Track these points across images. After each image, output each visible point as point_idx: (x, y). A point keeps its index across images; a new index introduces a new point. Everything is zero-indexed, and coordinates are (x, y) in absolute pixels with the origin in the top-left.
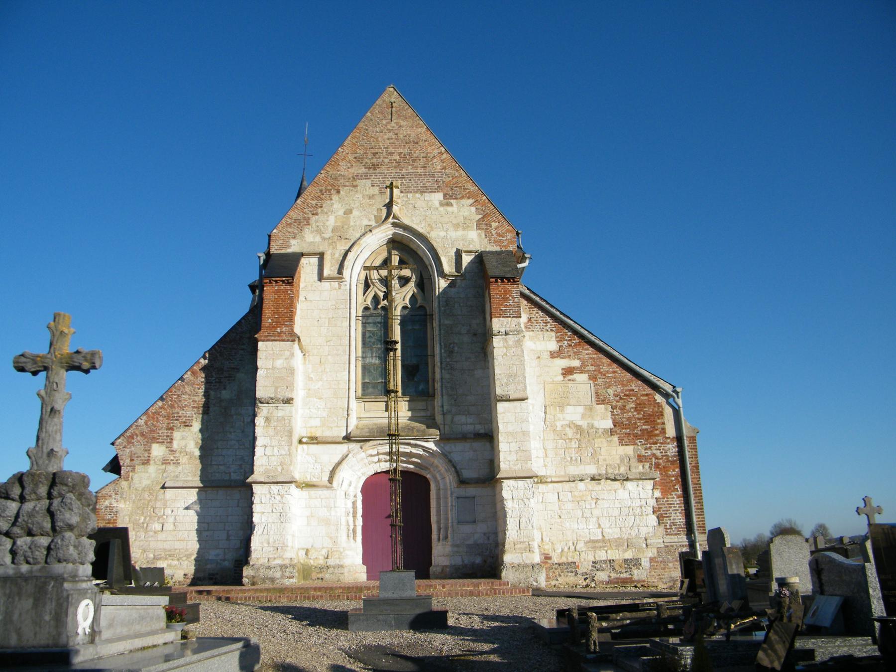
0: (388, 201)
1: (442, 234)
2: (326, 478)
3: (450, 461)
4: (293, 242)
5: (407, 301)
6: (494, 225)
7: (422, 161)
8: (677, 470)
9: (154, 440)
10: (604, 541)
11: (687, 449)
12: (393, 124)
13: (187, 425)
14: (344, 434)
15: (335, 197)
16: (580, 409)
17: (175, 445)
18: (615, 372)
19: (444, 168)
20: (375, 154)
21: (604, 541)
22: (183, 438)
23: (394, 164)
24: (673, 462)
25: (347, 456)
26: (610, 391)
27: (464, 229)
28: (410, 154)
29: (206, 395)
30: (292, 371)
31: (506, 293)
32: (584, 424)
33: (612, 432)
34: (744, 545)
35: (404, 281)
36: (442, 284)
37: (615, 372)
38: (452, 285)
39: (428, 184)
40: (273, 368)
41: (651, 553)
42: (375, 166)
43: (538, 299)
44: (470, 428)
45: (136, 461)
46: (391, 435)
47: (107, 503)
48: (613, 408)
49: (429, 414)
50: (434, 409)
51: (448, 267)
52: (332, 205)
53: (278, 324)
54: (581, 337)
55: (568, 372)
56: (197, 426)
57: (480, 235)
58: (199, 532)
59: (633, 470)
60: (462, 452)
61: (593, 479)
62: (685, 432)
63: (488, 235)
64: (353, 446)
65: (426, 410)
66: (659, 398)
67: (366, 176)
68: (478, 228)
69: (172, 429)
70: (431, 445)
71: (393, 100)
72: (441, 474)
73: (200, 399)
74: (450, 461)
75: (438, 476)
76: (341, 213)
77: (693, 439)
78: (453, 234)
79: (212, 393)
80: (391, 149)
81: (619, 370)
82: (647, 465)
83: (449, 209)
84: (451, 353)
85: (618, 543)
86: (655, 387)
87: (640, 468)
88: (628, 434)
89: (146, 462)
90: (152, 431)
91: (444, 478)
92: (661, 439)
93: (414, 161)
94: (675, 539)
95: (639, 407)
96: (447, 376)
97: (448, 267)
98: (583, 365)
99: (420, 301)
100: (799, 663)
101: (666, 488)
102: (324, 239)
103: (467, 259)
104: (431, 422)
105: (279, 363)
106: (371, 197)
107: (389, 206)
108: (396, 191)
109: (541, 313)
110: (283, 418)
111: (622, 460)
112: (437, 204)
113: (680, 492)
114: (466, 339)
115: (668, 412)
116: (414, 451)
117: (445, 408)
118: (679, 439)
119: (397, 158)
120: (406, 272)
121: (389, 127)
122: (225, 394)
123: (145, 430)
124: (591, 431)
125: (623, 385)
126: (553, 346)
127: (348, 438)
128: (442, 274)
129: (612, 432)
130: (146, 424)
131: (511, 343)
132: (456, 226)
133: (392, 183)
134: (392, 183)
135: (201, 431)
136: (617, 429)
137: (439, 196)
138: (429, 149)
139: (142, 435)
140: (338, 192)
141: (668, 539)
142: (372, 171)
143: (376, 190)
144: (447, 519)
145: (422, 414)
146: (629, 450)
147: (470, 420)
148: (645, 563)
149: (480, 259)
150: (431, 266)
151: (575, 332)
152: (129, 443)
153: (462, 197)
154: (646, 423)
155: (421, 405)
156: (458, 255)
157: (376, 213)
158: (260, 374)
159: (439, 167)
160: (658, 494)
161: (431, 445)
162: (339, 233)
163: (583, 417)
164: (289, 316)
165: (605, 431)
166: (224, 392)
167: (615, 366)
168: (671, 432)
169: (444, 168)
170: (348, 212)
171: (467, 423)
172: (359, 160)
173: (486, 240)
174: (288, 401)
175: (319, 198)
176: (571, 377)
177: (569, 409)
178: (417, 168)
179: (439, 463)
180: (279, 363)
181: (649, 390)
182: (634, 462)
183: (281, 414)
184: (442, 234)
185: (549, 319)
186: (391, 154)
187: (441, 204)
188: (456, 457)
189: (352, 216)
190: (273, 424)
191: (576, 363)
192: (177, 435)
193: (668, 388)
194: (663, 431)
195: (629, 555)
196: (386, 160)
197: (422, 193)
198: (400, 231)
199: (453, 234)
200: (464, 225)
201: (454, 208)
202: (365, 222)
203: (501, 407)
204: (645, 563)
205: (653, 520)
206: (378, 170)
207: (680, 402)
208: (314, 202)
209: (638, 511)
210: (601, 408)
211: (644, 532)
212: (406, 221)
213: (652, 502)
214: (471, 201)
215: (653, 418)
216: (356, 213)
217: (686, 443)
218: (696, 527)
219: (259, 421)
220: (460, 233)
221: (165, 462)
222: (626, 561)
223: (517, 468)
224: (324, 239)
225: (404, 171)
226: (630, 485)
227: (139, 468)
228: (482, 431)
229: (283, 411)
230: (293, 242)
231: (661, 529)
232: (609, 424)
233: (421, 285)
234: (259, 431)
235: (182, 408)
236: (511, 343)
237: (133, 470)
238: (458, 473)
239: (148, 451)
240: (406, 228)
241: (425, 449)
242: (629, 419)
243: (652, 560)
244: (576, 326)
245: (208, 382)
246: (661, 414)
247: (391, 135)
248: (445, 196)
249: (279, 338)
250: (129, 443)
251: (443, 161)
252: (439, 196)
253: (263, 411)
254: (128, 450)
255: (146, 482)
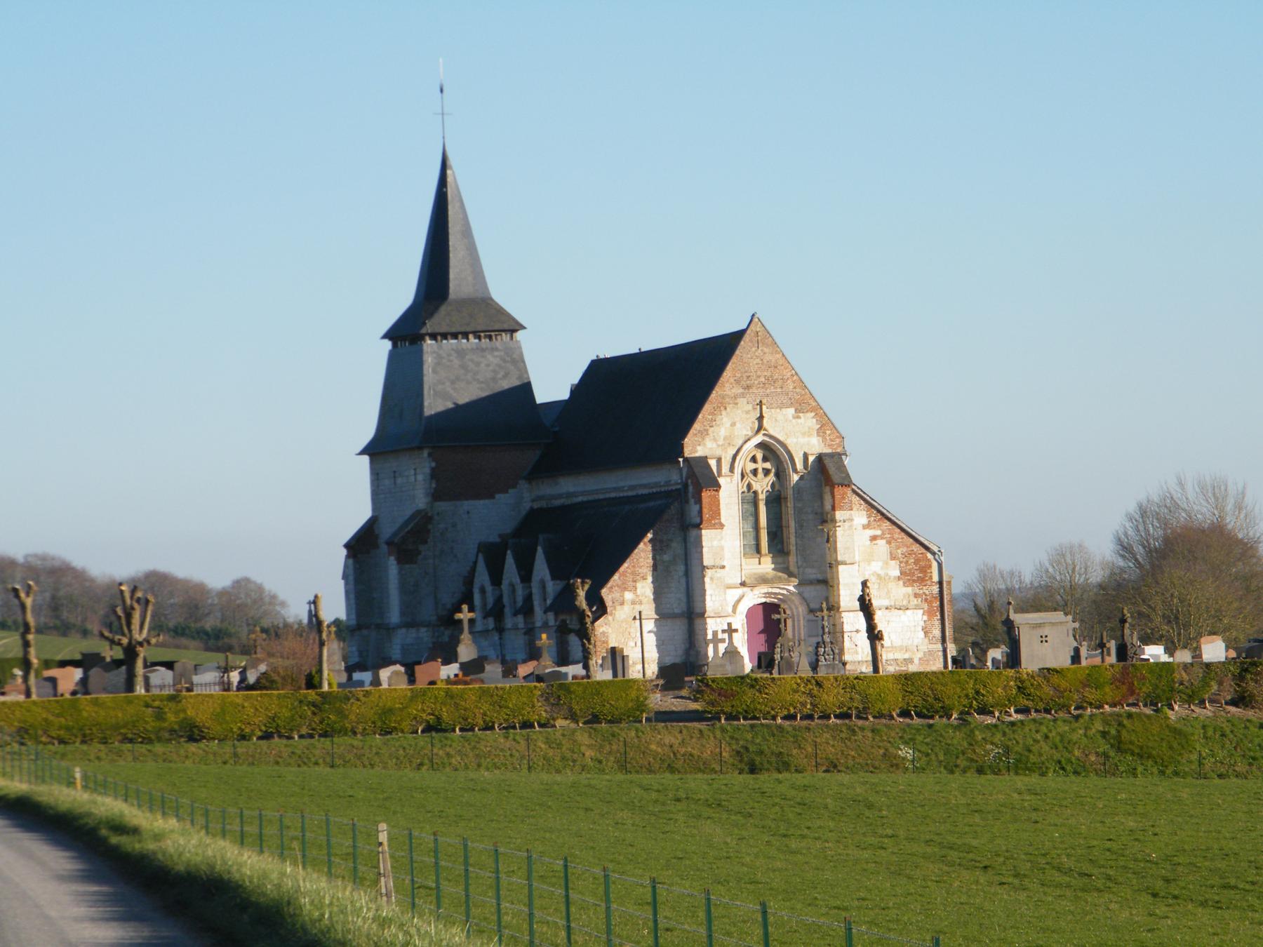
0: (758, 415)
1: (795, 440)
2: (730, 609)
3: (804, 598)
4: (699, 448)
5: (769, 488)
6: (828, 432)
7: (780, 382)
8: (938, 603)
9: (625, 589)
10: (892, 647)
11: (945, 589)
12: (759, 351)
13: (644, 578)
14: (740, 582)
15: (724, 413)
16: (880, 564)
17: (639, 591)
18: (902, 538)
19: (795, 388)
20: (748, 377)
21: (892, 647)
22: (643, 587)
23: (762, 385)
24: (936, 597)
25: (743, 596)
26: (899, 551)
27: (809, 436)
28: (771, 376)
29: (654, 558)
30: (722, 548)
31: (844, 494)
32: (882, 573)
33: (899, 578)
34: (983, 603)
35: (767, 472)
36: (795, 478)
37: (902, 538)
38: (801, 478)
39: (784, 401)
40: (712, 546)
41: (920, 655)
42: (748, 387)
43: (868, 498)
44: (813, 577)
45: (616, 603)
46: (763, 580)
47: (601, 630)
48: (901, 562)
49: (785, 566)
50: (789, 562)
51: (800, 466)
52: (722, 419)
53: (713, 518)
54: (882, 514)
55: (874, 538)
56: (650, 579)
57: (819, 441)
58: (658, 646)
59: (911, 603)
60: (810, 591)
61: (887, 608)
62: (945, 579)
63: (824, 440)
64: (745, 589)
65: (784, 563)
66: (929, 556)
67: (743, 395)
68: (818, 435)
69: (635, 581)
70: (791, 588)
71: (758, 330)
72: (795, 605)
73: (650, 561)
74: (804, 598)
75: (793, 607)
76: (728, 425)
77: (949, 583)
78: (803, 440)
79: (658, 557)
80: (759, 373)
81: (905, 537)
82: (920, 600)
83: (799, 421)
84: (801, 526)
85: (901, 649)
86: (927, 548)
87: (915, 602)
88: (909, 580)
89: (622, 604)
90: (623, 583)
91: (797, 608)
92: (929, 583)
93: (774, 382)
94: (935, 646)
95: (917, 562)
96: (799, 542)
97: (800, 466)
98: (883, 534)
99: (777, 487)
100: (498, 540)
101: (929, 613)
102: (718, 446)
103: (811, 459)
104: (791, 575)
105: (715, 543)
106: (747, 412)
107: (761, 418)
108: (764, 407)
109: (858, 498)
110: (720, 578)
111: (904, 596)
112: (791, 418)
113: (939, 617)
114: (811, 517)
115: (935, 565)
116: (782, 592)
117: (800, 563)
118: (940, 583)
119: (763, 380)
120: (768, 465)
121: (757, 354)
122: (666, 557)
123: (620, 583)
124: (887, 578)
125: (908, 547)
126: (865, 521)
127: (743, 584)
128: (795, 471)
129: (899, 578)
130: (619, 578)
131: (846, 527)
132: (804, 434)
133: (761, 402)
134: (761, 402)
135: (652, 582)
136: (902, 577)
137: (791, 411)
138: (785, 373)
139: (618, 586)
140: (726, 409)
141: (931, 647)
142: (747, 391)
143: (750, 407)
144: (800, 634)
145: (782, 566)
146: (909, 590)
147: (814, 571)
148: (916, 661)
149: (820, 458)
150: (787, 464)
151: (879, 511)
152: (610, 591)
153: (807, 412)
154: (921, 572)
155: (780, 560)
156: (806, 456)
157: (751, 425)
158: (705, 550)
159: (791, 387)
160: (925, 618)
161: (791, 588)
162: (729, 440)
163: (882, 568)
164: (717, 513)
165: (895, 577)
166: (665, 556)
167: (903, 534)
168: (936, 578)
169: (795, 388)
170: (733, 424)
171: (812, 573)
172: (738, 382)
173: (823, 445)
174: (723, 567)
175: (712, 414)
176: (875, 542)
177: (873, 564)
178: (776, 388)
179: (797, 600)
180: (715, 543)
181: (923, 551)
182: (912, 598)
183: (718, 575)
184: (795, 440)
185: (862, 502)
186: (759, 377)
187: (794, 418)
188: (806, 595)
189: (735, 427)
190: (715, 581)
191: (879, 532)
192: (639, 585)
193: (935, 549)
194: (931, 578)
195: (907, 656)
196: (756, 382)
197: (781, 408)
198: (767, 439)
199: (803, 440)
200: (807, 434)
201: (801, 421)
202: (745, 432)
203: (841, 568)
204: (916, 661)
205: (922, 634)
206: (751, 391)
207: (942, 558)
208: (710, 417)
209: (913, 629)
210: (893, 562)
211: (916, 642)
212: (772, 432)
213: (922, 623)
214: (813, 414)
215: (925, 569)
216: (738, 425)
217: (945, 585)
218: (947, 639)
219: (707, 580)
220: (806, 439)
221: (633, 603)
222: (905, 659)
223: (850, 605)
224: (718, 446)
225: (768, 391)
226: (909, 612)
227: (618, 607)
228: (821, 578)
229: (721, 573)
230: (699, 448)
231: (927, 640)
232: (897, 573)
233: (777, 475)
234: (707, 586)
235: (641, 567)
236: (846, 527)
237: (615, 609)
238: (808, 605)
239: (623, 596)
240: (771, 437)
241: (788, 590)
242: (910, 570)
243: (920, 659)
244: (879, 507)
245: (654, 550)
246: (930, 566)
247: (758, 361)
248: (796, 410)
249: (714, 527)
250: (610, 591)
251: (794, 382)
252: (791, 411)
253: (709, 573)
254: (610, 597)
255: (623, 616)
